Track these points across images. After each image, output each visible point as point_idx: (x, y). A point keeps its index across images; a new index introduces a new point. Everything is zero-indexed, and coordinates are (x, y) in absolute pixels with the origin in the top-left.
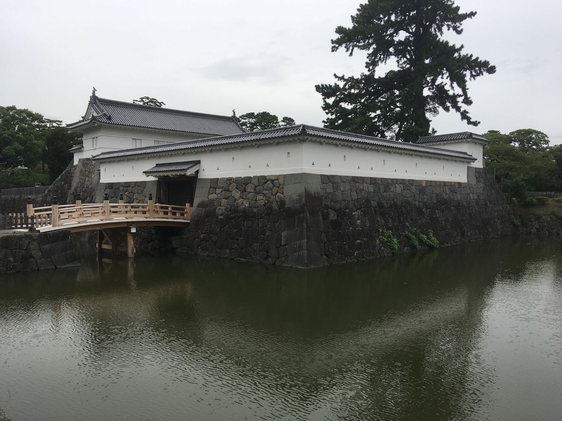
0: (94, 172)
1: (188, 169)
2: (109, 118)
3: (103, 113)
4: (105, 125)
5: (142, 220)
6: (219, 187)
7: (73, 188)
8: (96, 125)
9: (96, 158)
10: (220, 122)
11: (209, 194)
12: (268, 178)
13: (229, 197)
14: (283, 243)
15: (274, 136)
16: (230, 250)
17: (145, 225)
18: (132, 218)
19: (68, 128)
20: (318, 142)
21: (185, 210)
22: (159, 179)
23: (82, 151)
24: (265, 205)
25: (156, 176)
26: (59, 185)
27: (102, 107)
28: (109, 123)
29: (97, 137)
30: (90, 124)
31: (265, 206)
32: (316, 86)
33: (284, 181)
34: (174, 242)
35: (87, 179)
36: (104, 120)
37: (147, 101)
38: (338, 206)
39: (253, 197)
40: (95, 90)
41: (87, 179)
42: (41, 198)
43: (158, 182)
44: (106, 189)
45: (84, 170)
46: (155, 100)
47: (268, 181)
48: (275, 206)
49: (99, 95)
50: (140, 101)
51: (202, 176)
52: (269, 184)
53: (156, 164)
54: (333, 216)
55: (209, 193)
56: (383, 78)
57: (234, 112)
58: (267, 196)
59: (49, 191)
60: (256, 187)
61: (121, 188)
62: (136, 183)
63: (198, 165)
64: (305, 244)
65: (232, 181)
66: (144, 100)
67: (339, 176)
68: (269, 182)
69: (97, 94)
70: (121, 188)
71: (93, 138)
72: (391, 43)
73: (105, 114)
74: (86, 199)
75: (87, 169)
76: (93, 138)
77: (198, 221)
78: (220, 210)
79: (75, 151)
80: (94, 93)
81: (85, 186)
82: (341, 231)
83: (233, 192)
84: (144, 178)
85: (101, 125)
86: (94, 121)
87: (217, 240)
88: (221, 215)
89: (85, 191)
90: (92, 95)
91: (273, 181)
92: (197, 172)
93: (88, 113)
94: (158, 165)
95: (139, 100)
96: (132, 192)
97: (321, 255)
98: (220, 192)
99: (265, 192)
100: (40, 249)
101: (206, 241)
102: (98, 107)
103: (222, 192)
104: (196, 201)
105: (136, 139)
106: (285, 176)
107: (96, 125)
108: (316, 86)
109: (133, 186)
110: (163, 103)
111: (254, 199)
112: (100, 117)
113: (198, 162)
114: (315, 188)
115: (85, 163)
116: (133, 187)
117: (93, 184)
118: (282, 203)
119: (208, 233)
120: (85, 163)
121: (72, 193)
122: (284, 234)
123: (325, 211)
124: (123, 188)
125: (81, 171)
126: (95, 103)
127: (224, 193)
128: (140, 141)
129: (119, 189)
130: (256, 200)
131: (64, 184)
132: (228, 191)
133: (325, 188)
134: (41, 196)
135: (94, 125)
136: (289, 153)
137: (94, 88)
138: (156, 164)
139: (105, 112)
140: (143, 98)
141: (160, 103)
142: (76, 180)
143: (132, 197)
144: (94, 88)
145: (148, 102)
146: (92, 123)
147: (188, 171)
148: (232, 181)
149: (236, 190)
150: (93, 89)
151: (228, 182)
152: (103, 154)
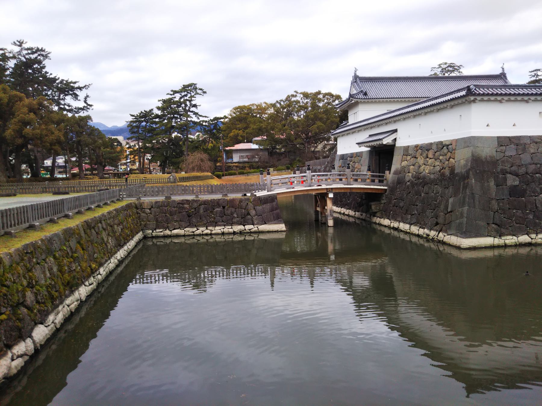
1: (384, 138)
2: (365, 94)
3: (361, 90)
5: (342, 187)
6: (409, 154)
11: (402, 161)
12: (444, 143)
13: (415, 164)
14: (449, 210)
16: (411, 215)
17: (343, 191)
18: (331, 185)
20: (492, 101)
21: (384, 177)
22: (371, 148)
24: (440, 171)
25: (367, 147)
28: (364, 99)
29: (356, 113)
30: (349, 102)
31: (440, 172)
33: (456, 145)
34: (373, 207)
36: (361, 96)
37: (445, 66)
38: (522, 171)
39: (432, 164)
43: (370, 152)
44: (340, 159)
46: (453, 64)
47: (444, 146)
48: (447, 172)
49: (361, 74)
50: (438, 68)
51: (398, 144)
52: (445, 150)
54: (512, 181)
55: (402, 160)
57: (503, 69)
58: (442, 161)
60: (435, 152)
61: (349, 159)
63: (396, 133)
64: (465, 212)
65: (419, 147)
66: (442, 66)
67: (529, 136)
68: (445, 147)
69: (358, 74)
70: (349, 159)
71: (355, 114)
72: (60, 84)
73: (362, 90)
76: (355, 114)
77: (393, 189)
78: (409, 176)
80: (355, 74)
82: (524, 198)
83: (419, 159)
84: (357, 149)
85: (357, 101)
86: (351, 99)
88: (408, 182)
91: (448, 145)
92: (395, 139)
94: (370, 136)
95: (438, 67)
96: (354, 162)
97: (488, 224)
99: (441, 158)
100: (255, 209)
101: (396, 207)
104: (393, 168)
106: (457, 141)
109: (355, 156)
110: (462, 66)
111: (433, 165)
112: (357, 94)
113: (396, 131)
114: (487, 151)
118: (452, 169)
122: (451, 200)
123: (501, 176)
126: (356, 82)
127: (412, 159)
130: (434, 166)
132: (415, 158)
133: (503, 151)
135: (351, 102)
137: (356, 68)
140: (441, 64)
141: (459, 67)
144: (356, 68)
145: (446, 67)
147: (384, 140)
148: (419, 147)
150: (355, 69)
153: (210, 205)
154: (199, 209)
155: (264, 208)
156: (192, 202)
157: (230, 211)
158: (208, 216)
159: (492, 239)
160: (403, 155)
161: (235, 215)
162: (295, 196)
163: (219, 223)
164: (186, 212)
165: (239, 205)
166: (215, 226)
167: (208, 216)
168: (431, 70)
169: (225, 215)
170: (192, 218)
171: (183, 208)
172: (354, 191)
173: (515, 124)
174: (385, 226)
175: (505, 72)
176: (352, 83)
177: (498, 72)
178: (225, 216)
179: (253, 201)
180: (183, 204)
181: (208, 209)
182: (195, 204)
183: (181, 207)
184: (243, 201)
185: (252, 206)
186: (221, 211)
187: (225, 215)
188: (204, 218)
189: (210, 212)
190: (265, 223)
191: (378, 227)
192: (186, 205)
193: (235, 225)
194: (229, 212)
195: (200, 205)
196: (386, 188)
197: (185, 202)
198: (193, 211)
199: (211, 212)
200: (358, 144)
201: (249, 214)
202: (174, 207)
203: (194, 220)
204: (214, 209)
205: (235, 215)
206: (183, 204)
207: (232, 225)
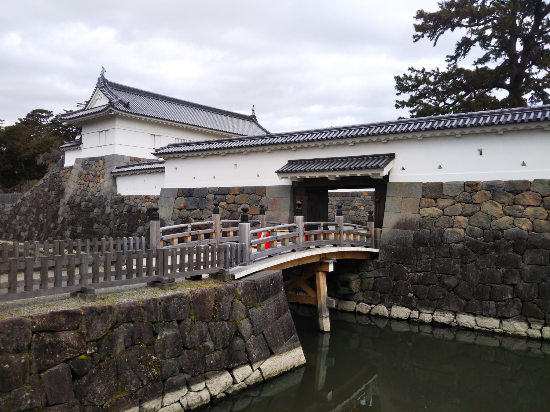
0: (103, 176)
2: (127, 106)
4: (128, 116)
7: (67, 197)
8: (113, 113)
9: (161, 152)
10: (241, 121)
15: (237, 145)
19: (62, 118)
23: (80, 149)
26: (40, 191)
27: (115, 92)
32: (395, 77)
35: (91, 184)
40: (104, 71)
41: (91, 184)
42: (11, 208)
45: (85, 172)
53: (289, 161)
56: (493, 70)
59: (24, 199)
62: (242, 190)
69: (106, 76)
70: (211, 197)
74: (93, 211)
75: (90, 172)
76: (100, 132)
79: (66, 149)
80: (102, 76)
81: (89, 194)
86: (111, 108)
87: (458, 284)
89: (90, 200)
90: (100, 76)
93: (94, 99)
94: (290, 162)
98: (450, 204)
102: (110, 92)
103: (453, 204)
105: (154, 135)
107: (113, 113)
108: (395, 77)
109: (237, 193)
115: (88, 164)
116: (236, 195)
117: (103, 191)
119: (429, 271)
120: (86, 163)
121: (66, 202)
124: (213, 196)
125: (80, 174)
128: (159, 137)
129: (205, 197)
131: (48, 191)
134: (10, 205)
135: (110, 114)
136: (236, 165)
138: (289, 161)
139: (121, 98)
142: (72, 186)
143: (235, 209)
146: (108, 110)
149: (491, 202)
150: (102, 69)
151: (469, 189)
152: (170, 146)
153: (145, 322)
154: (112, 341)
155: (266, 311)
156: (89, 318)
157: (197, 333)
158: (141, 361)
159: (407, 310)
160: (423, 197)
161: (210, 344)
162: (284, 271)
163: (175, 379)
164: (66, 361)
165: (214, 310)
166: (163, 394)
167: (141, 361)
168: (77, 106)
169: (185, 348)
170: (90, 382)
171: (56, 347)
172: (347, 257)
173: (525, 165)
174: (350, 312)
175: (256, 115)
176: (96, 88)
177: (249, 113)
178: (185, 352)
179: (244, 295)
180: (52, 331)
181: (141, 339)
182: (99, 326)
183: (46, 346)
184: (224, 298)
185: (244, 307)
186: (176, 335)
187: (185, 348)
188: (129, 374)
189: (147, 345)
190: (272, 354)
191: (351, 319)
192: (67, 334)
193: (214, 375)
194: (195, 336)
195: (112, 328)
196: (376, 250)
197: (63, 319)
198: (91, 355)
199: (151, 345)
200: (278, 172)
201: (238, 334)
202: (18, 351)
203: (99, 390)
204: (155, 335)
205: (210, 344)
206: (52, 331)
207: (206, 378)
